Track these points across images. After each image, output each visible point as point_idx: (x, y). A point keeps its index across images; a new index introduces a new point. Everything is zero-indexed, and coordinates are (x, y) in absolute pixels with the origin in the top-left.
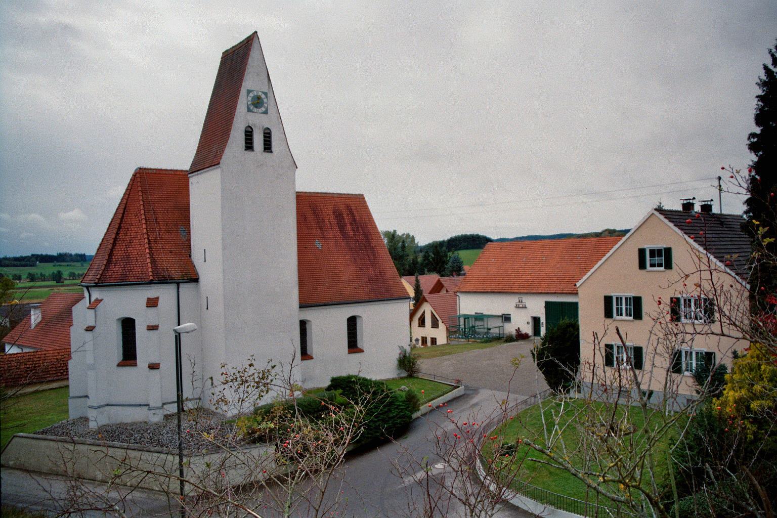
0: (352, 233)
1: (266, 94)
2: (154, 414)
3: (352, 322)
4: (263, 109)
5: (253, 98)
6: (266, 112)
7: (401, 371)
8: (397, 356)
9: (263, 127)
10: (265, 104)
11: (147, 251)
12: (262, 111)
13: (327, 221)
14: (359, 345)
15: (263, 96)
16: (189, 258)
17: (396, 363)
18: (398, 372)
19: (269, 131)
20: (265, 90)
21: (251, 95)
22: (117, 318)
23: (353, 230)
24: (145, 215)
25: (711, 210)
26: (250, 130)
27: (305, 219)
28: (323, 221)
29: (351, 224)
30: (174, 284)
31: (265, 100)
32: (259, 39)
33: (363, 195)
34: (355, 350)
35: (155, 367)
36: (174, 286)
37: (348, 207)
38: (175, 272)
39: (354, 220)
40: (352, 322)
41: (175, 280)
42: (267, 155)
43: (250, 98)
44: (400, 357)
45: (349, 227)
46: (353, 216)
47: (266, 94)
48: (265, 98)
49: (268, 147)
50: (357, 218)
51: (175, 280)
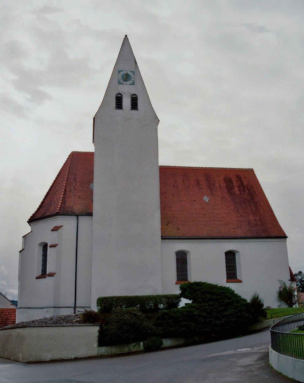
0: (238, 193)
1: (133, 72)
2: (47, 311)
3: (231, 256)
4: (131, 82)
5: (123, 75)
6: (133, 84)
7: (281, 303)
8: (278, 290)
9: (131, 93)
10: (132, 79)
11: (62, 196)
12: (130, 83)
13: (217, 185)
14: (238, 278)
15: (131, 74)
16: (92, 201)
17: (277, 295)
18: (278, 304)
19: (136, 96)
20: (133, 70)
21: (122, 73)
22: (39, 243)
23: (239, 190)
24: (68, 176)
25: (101, 332)
26: (120, 96)
27: (198, 183)
28: (214, 184)
29: (238, 187)
30: (74, 217)
31: (133, 76)
32: (128, 39)
33: (253, 169)
34: (234, 280)
35: (50, 275)
36: (75, 218)
37: (239, 178)
38: (77, 208)
39: (242, 184)
40: (231, 256)
41: (75, 213)
42: (134, 112)
43: (120, 75)
44: (280, 291)
45: (236, 189)
46: (242, 182)
47: (133, 72)
48: (132, 75)
49: (134, 105)
50: (245, 184)
51: (75, 213)
